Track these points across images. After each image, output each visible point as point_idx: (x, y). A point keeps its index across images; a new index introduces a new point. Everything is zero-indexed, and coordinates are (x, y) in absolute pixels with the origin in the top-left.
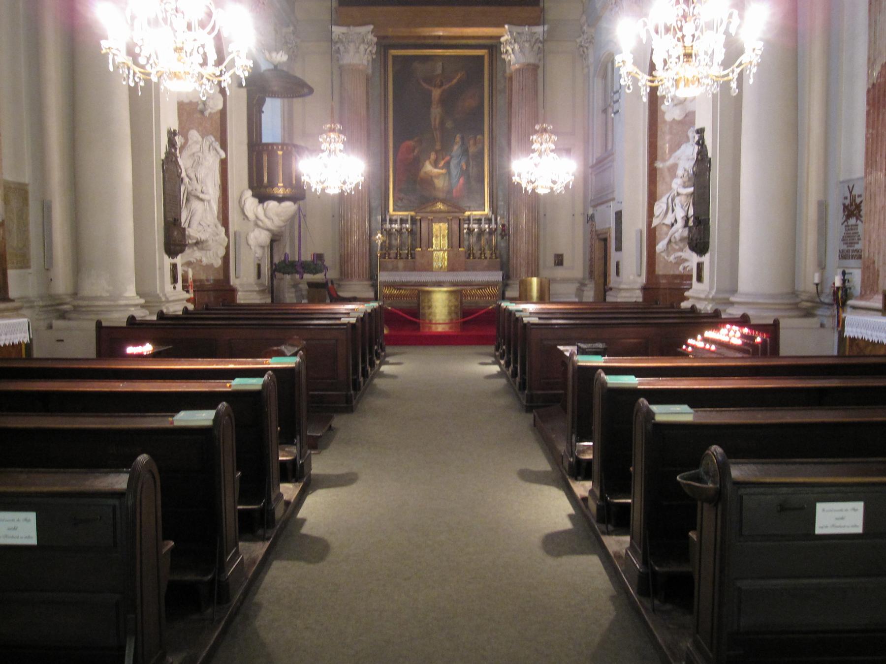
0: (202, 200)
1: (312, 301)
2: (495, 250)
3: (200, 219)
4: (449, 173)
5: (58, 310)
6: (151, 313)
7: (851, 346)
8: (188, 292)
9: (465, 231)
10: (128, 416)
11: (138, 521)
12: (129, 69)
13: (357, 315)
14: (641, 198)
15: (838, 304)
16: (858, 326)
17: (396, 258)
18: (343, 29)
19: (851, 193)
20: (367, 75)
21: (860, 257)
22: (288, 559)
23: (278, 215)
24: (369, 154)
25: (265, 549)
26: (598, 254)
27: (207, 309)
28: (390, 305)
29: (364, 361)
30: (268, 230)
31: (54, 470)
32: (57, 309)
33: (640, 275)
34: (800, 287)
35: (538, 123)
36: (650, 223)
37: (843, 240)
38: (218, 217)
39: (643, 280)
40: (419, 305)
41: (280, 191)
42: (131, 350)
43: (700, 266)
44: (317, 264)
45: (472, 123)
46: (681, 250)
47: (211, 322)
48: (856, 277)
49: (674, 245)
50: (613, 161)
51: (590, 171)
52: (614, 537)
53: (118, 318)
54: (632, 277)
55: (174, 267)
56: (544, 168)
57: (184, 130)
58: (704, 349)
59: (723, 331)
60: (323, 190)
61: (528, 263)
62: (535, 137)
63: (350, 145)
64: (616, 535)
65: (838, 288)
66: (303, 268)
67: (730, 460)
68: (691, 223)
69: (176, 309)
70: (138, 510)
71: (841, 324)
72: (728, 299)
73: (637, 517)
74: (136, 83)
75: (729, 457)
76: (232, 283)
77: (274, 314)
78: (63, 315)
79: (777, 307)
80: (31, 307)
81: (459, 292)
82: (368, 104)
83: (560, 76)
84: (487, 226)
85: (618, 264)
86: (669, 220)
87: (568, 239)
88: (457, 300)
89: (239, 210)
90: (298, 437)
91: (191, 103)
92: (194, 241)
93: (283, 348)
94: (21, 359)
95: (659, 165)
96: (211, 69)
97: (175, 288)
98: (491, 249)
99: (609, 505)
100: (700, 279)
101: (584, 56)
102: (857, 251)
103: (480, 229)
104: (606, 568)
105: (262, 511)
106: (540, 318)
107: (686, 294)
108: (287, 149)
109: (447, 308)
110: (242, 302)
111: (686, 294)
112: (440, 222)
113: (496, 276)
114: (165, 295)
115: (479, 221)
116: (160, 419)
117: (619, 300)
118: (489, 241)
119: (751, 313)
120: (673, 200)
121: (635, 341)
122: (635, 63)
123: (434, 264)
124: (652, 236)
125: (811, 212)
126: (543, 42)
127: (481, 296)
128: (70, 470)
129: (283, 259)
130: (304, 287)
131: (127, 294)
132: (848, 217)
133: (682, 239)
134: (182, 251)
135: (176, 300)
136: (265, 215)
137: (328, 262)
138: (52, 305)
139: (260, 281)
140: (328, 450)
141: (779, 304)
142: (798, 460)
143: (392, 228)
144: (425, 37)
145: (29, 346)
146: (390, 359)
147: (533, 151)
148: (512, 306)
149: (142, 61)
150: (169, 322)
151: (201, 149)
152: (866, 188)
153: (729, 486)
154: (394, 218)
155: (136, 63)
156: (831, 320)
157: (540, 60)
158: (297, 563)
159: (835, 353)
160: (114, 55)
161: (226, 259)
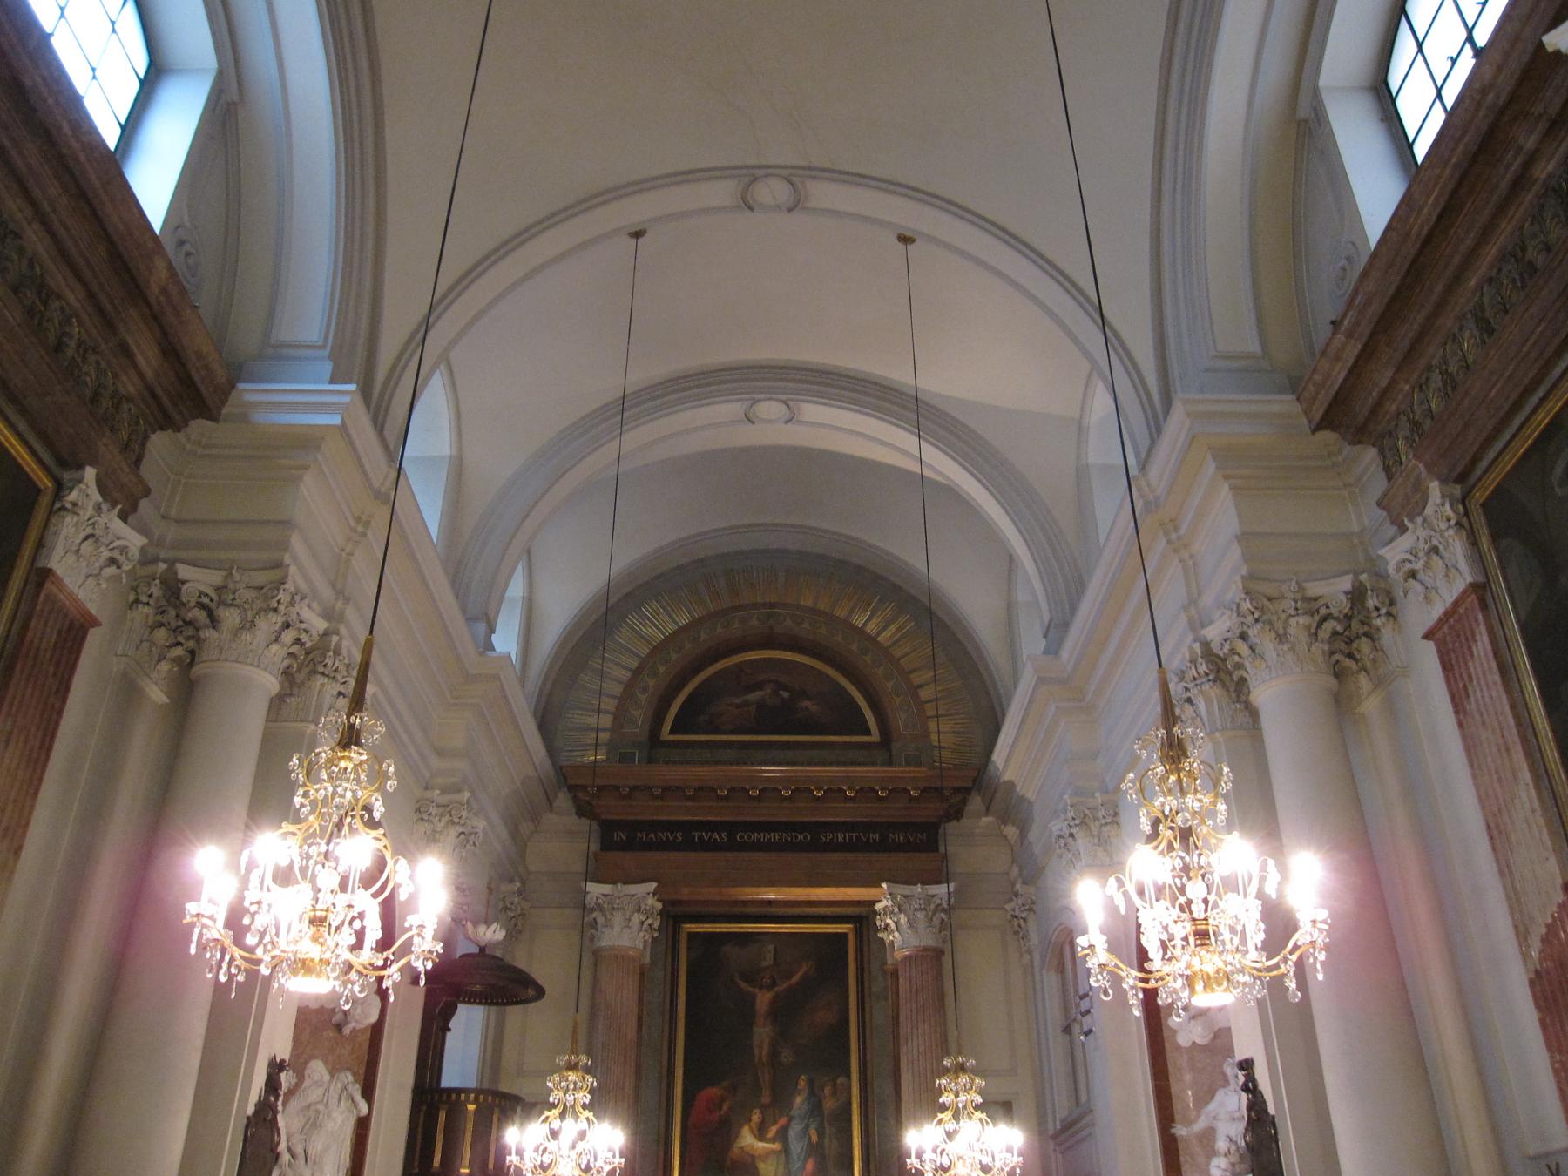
4: (786, 1150)
12: (223, 951)
18: (606, 888)
20: (642, 967)
35: (948, 1054)
45: (829, 1054)
57: (298, 1062)
74: (231, 977)
83: (984, 975)
91: (321, 1011)
96: (367, 955)
101: (1020, 934)
122: (1112, 948)
126: (949, 911)
144: (745, 903)
149: (251, 940)
155: (238, 941)
160: (204, 926)
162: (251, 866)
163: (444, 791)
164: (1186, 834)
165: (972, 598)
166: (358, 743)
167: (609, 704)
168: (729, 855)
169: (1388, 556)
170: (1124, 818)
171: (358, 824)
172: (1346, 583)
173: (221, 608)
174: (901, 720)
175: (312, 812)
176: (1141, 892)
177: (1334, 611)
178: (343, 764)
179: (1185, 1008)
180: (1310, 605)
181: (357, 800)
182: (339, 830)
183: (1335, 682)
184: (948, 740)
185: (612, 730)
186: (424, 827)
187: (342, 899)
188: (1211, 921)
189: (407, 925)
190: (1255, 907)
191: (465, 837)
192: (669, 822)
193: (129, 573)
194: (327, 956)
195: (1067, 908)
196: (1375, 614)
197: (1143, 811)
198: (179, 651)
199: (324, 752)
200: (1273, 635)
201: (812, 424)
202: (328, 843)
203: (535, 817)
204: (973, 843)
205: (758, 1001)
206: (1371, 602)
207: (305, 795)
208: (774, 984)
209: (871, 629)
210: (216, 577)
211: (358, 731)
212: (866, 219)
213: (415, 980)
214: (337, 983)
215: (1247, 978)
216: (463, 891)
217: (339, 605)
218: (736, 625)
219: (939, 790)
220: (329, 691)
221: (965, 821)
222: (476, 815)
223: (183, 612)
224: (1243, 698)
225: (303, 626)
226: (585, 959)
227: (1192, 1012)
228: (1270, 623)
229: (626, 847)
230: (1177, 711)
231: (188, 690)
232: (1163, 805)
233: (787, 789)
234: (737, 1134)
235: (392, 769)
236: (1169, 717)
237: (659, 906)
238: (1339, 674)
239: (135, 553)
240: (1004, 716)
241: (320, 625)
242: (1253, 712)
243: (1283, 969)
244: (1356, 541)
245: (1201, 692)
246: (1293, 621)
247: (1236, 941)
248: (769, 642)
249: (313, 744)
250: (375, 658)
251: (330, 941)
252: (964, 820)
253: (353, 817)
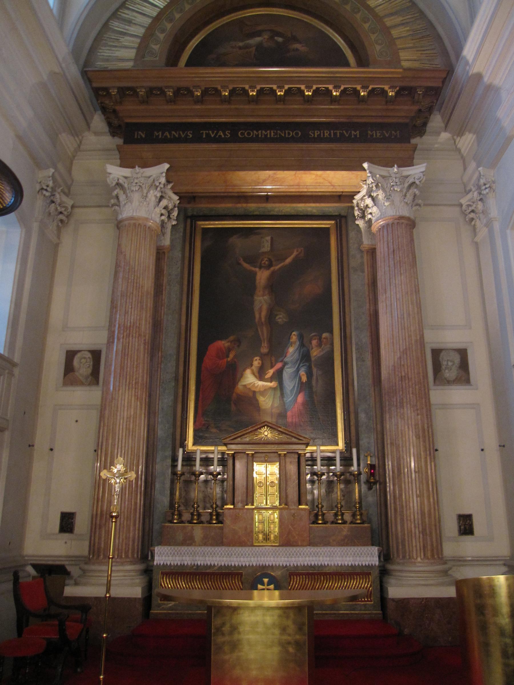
113: (368, 556)
115: (329, 461)
118: (348, 494)
205: (258, 277)
208: (270, 265)
234: (242, 376)
252: (424, 137)
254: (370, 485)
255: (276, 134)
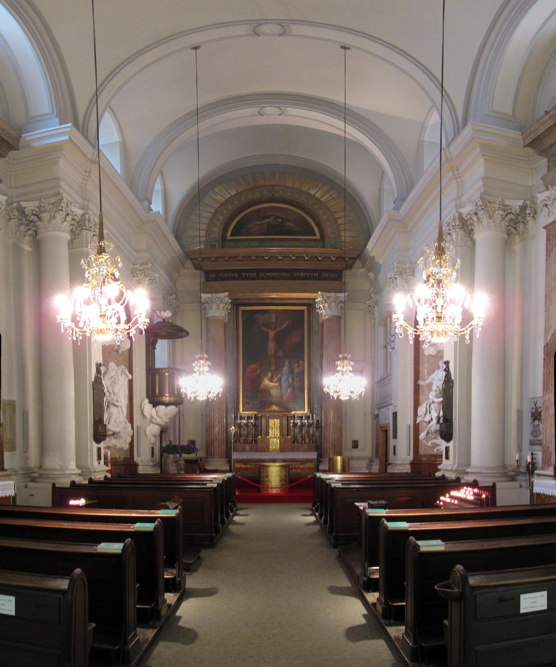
0: (117, 406)
1: (187, 472)
2: (312, 438)
3: (115, 418)
4: (280, 385)
5: (31, 477)
6: (85, 479)
7: (537, 498)
8: (107, 466)
9: (292, 425)
10: (69, 544)
11: (74, 609)
12: (73, 330)
13: (217, 482)
14: (409, 404)
15: (529, 472)
16: (541, 486)
17: (244, 443)
18: (209, 295)
19: (535, 405)
20: (225, 323)
21: (541, 444)
22: (169, 641)
23: (165, 415)
24: (226, 374)
25: (154, 634)
26: (382, 440)
27: (119, 477)
28: (240, 475)
29: (222, 513)
30: (159, 425)
31: (26, 573)
32: (30, 476)
33: (409, 455)
34: (508, 462)
35: (341, 353)
36: (415, 420)
37: (532, 434)
38: (127, 417)
39: (411, 458)
40: (260, 475)
41: (167, 399)
42: (72, 502)
43: (447, 449)
44: (191, 447)
45: (296, 352)
46: (435, 438)
47: (122, 485)
48: (539, 456)
49: (431, 435)
50: (391, 379)
51: (376, 385)
52: (394, 627)
53: (65, 482)
54: (404, 456)
55: (99, 449)
56: (344, 383)
57: (106, 363)
58: (450, 503)
59: (462, 491)
60: (195, 397)
61: (334, 447)
62: (339, 362)
63: (213, 368)
64: (396, 626)
65: (529, 463)
66: (181, 450)
67: (468, 574)
68: (441, 421)
69: (100, 477)
70: (74, 602)
71: (531, 485)
72: (465, 470)
73: (409, 614)
74: (77, 338)
75: (468, 572)
76: (135, 460)
77: (162, 481)
78: (33, 480)
79: (494, 475)
80: (16, 474)
81: (287, 466)
82: (225, 341)
83: (356, 323)
84: (306, 421)
85: (394, 447)
86: (427, 419)
87: (361, 430)
88: (286, 472)
89: (140, 412)
90: (177, 563)
91: (110, 346)
92: (112, 433)
93: (168, 503)
94: (10, 505)
95: (421, 383)
96: (123, 326)
97: (99, 463)
98: (309, 437)
99: (391, 607)
100: (447, 457)
101: (371, 312)
102: (539, 440)
103: (302, 423)
104: (389, 647)
105: (152, 610)
106: (343, 484)
107: (439, 467)
108: (172, 371)
109: (279, 477)
110: (142, 472)
111: (439, 467)
112: (274, 418)
113: (313, 455)
114: (93, 468)
115: (301, 418)
116: (89, 547)
117: (395, 471)
118: (308, 432)
119: (479, 479)
120: (430, 406)
121: (406, 498)
122: (405, 320)
123: (271, 447)
124: (417, 429)
125: (513, 416)
126: (344, 303)
127: (302, 469)
128: (35, 574)
129: (168, 444)
130: (182, 462)
131: (71, 467)
132: (534, 420)
133: (436, 431)
134: (104, 439)
135: (100, 471)
136: (157, 415)
137: (198, 445)
138: (27, 474)
139: (153, 459)
140: (197, 573)
141: (496, 473)
142: (509, 570)
143: (242, 423)
144: (264, 299)
145: (14, 498)
146: (240, 512)
147: (338, 371)
148: (324, 476)
149: (81, 325)
150: (96, 485)
151: (117, 374)
152: (544, 403)
153: (468, 590)
154: (243, 416)
155: (77, 326)
156: (526, 482)
157: (342, 314)
158: (175, 644)
159: (529, 503)
160: (64, 322)
161: (131, 444)
162: (75, 301)
163: (141, 265)
164: (439, 282)
165: (364, 186)
166: (104, 252)
167: (204, 227)
168: (257, 281)
169: (539, 197)
170: (416, 274)
171: (110, 280)
172: (521, 203)
173: (41, 214)
174: (329, 231)
175: (93, 278)
176: (419, 301)
177: (513, 212)
178: (100, 260)
179: (429, 342)
180: (505, 208)
181: (108, 272)
182: (104, 284)
183: (507, 236)
184: (348, 239)
185: (206, 236)
186: (135, 279)
187: (110, 307)
188: (443, 313)
189: (135, 314)
190: (460, 310)
191: (152, 281)
192: (232, 270)
193: (4, 210)
194: (108, 327)
195: (390, 304)
196: (528, 216)
197: (424, 272)
198: (30, 232)
199: (93, 257)
200: (488, 215)
201: (291, 116)
202: (101, 288)
203: (178, 271)
204: (355, 278)
206: (528, 211)
207: (89, 273)
209: (318, 195)
210: (36, 203)
211: (104, 248)
212: (323, 39)
213: (141, 333)
214: (114, 336)
215: (453, 335)
216: (154, 300)
217: (86, 203)
218: (257, 194)
219: (344, 258)
220: (89, 235)
221: (354, 270)
222: (155, 272)
223: (28, 218)
224: (471, 236)
225: (74, 213)
226: (203, 321)
227: (431, 344)
228: (488, 211)
229: (215, 279)
230: (444, 237)
231: (38, 245)
232: (432, 270)
233: (280, 256)
234: (263, 380)
235: (119, 259)
236: (440, 239)
237: (230, 301)
238: (509, 234)
239: (4, 202)
240: (373, 231)
241: (81, 212)
242: (473, 242)
243: (465, 332)
244: (529, 189)
245: (455, 231)
246: (497, 212)
247: (451, 321)
248: (272, 200)
249: (88, 255)
250: (105, 220)
251: (109, 322)
253: (108, 278)
254: (317, 428)
255: (278, 274)
